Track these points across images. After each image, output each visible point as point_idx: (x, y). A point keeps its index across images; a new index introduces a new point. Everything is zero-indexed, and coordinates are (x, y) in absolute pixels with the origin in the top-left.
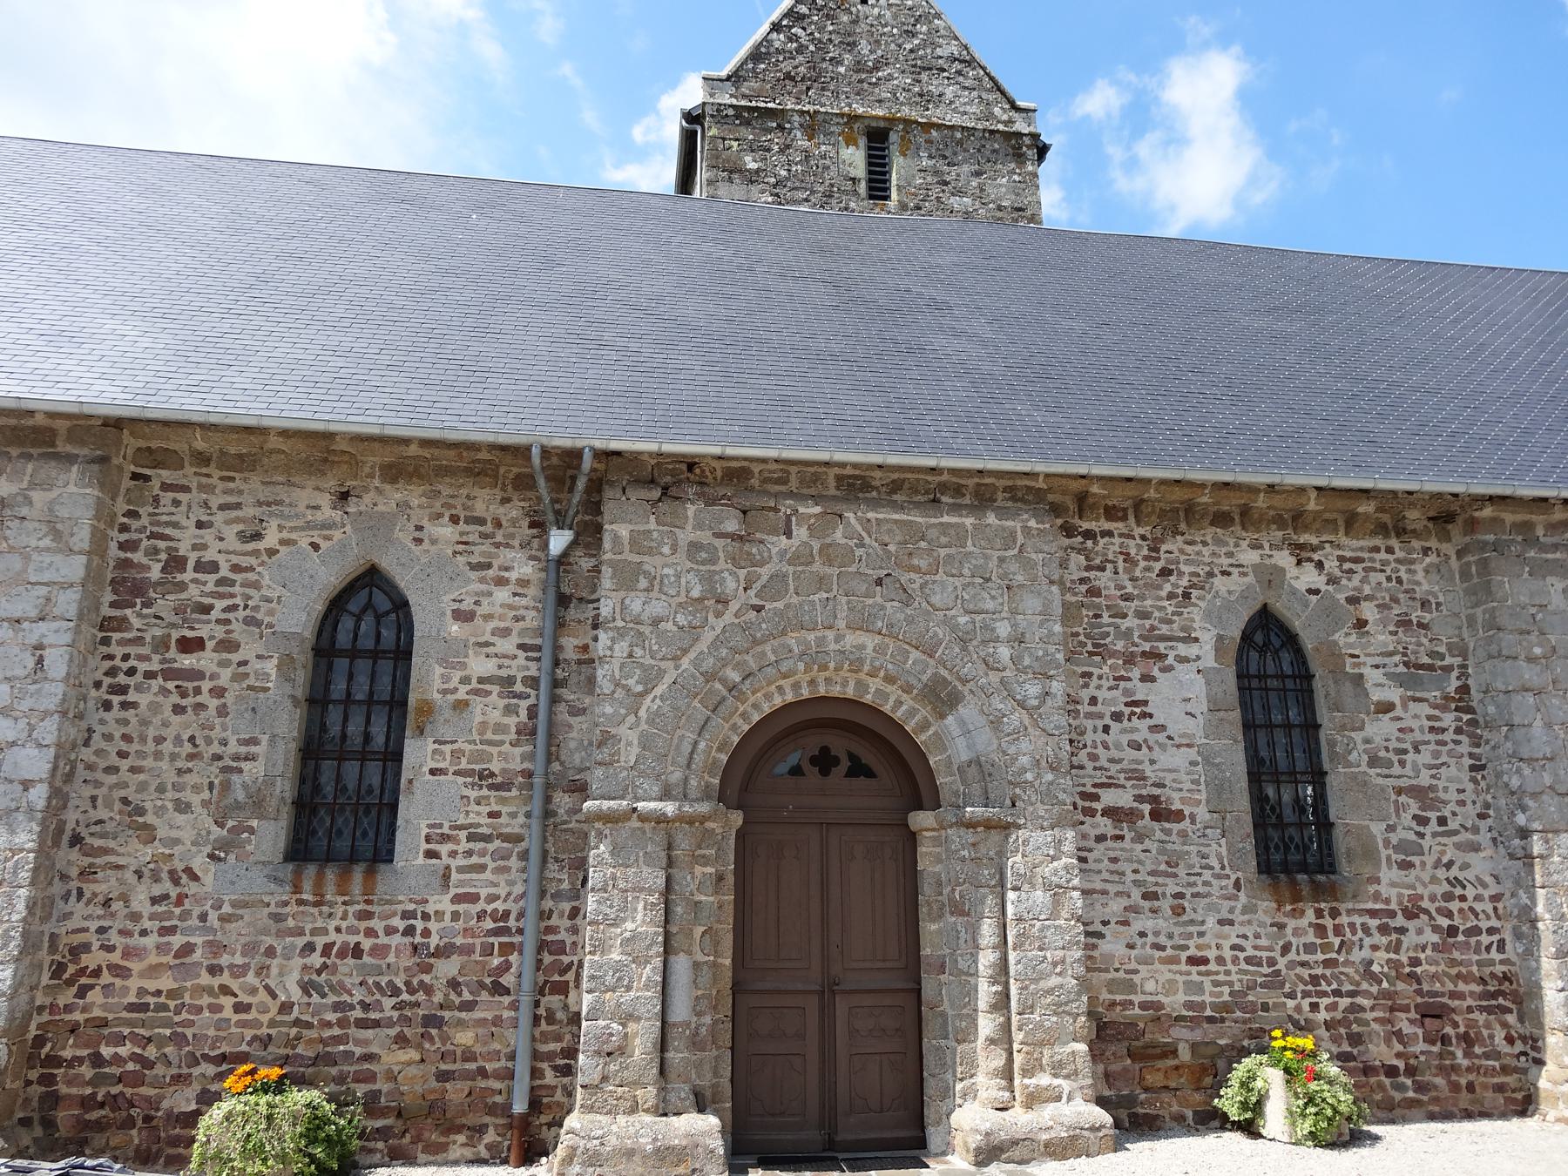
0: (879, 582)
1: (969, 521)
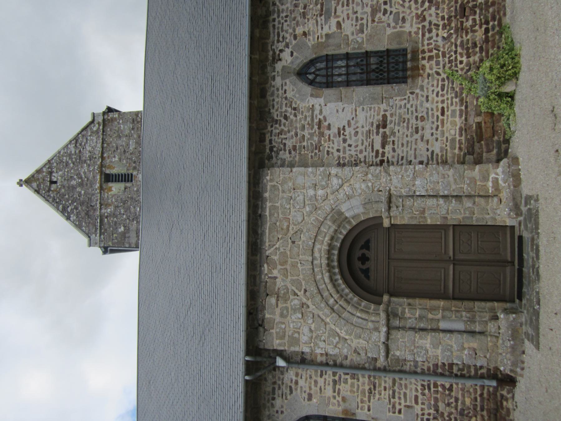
0: (293, 242)
1: (268, 204)
